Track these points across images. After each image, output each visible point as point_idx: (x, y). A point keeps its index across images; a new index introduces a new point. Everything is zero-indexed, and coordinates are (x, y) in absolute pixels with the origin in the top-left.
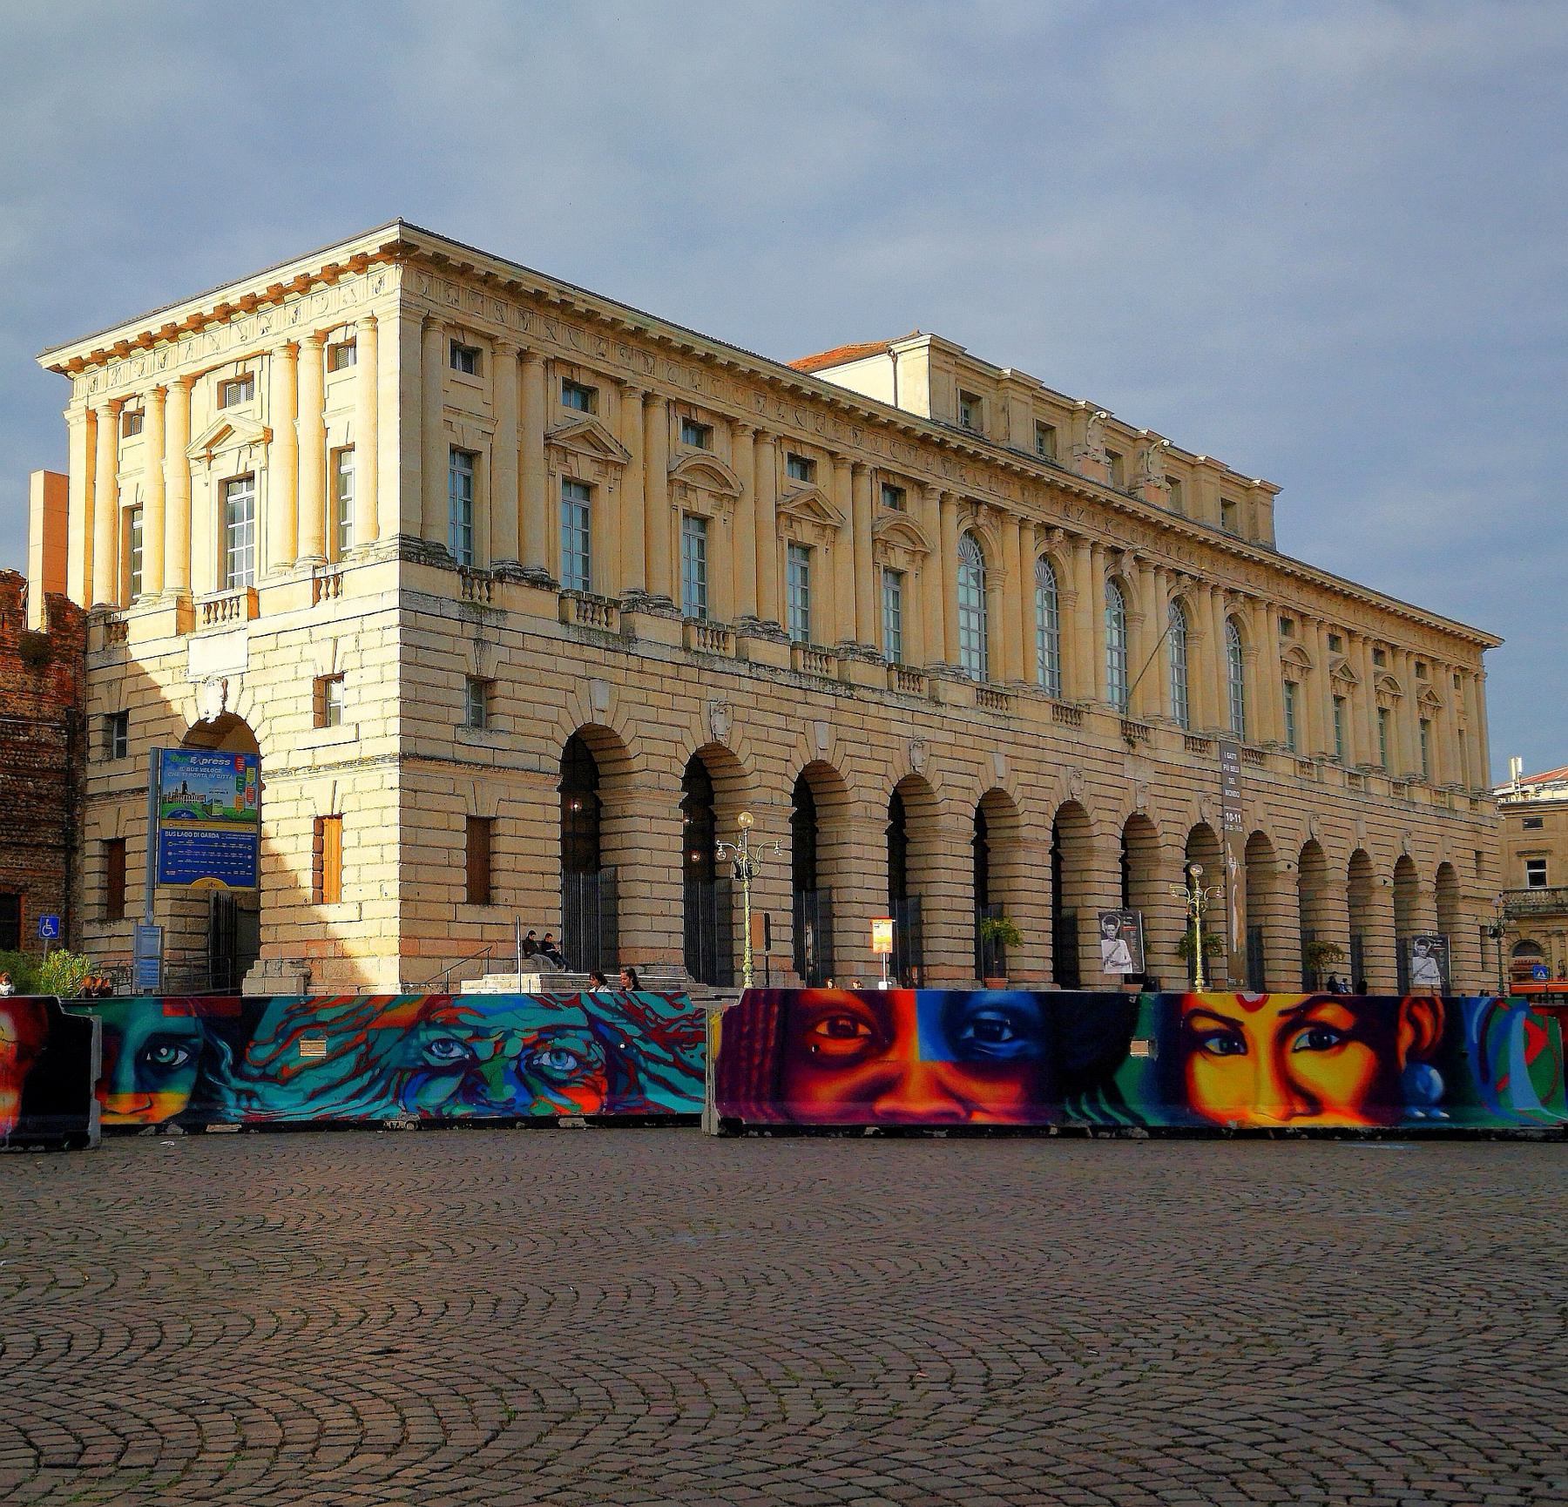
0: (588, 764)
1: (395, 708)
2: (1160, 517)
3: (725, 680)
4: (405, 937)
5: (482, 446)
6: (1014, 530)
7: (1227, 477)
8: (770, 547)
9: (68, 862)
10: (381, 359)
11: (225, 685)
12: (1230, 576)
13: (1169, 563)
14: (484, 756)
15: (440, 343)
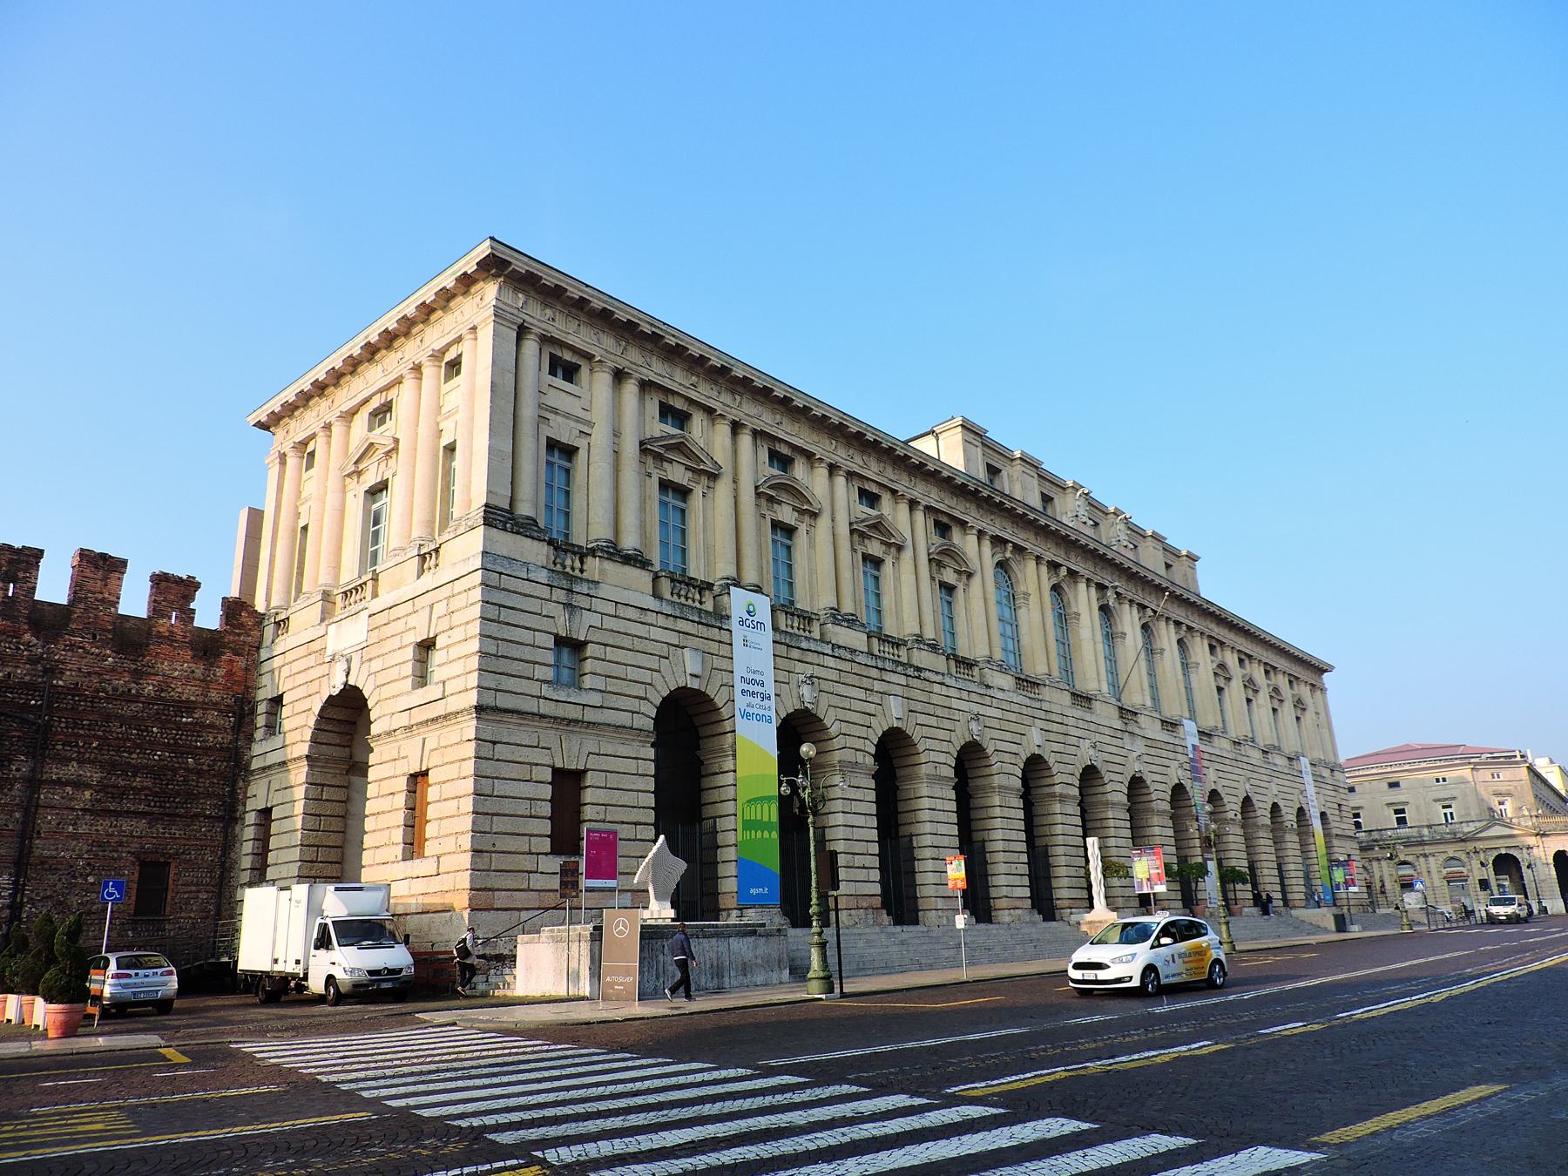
3: (811, 657)
5: (581, 443)
10: (480, 358)
11: (349, 661)
12: (1178, 613)
13: (1139, 599)
14: (573, 713)
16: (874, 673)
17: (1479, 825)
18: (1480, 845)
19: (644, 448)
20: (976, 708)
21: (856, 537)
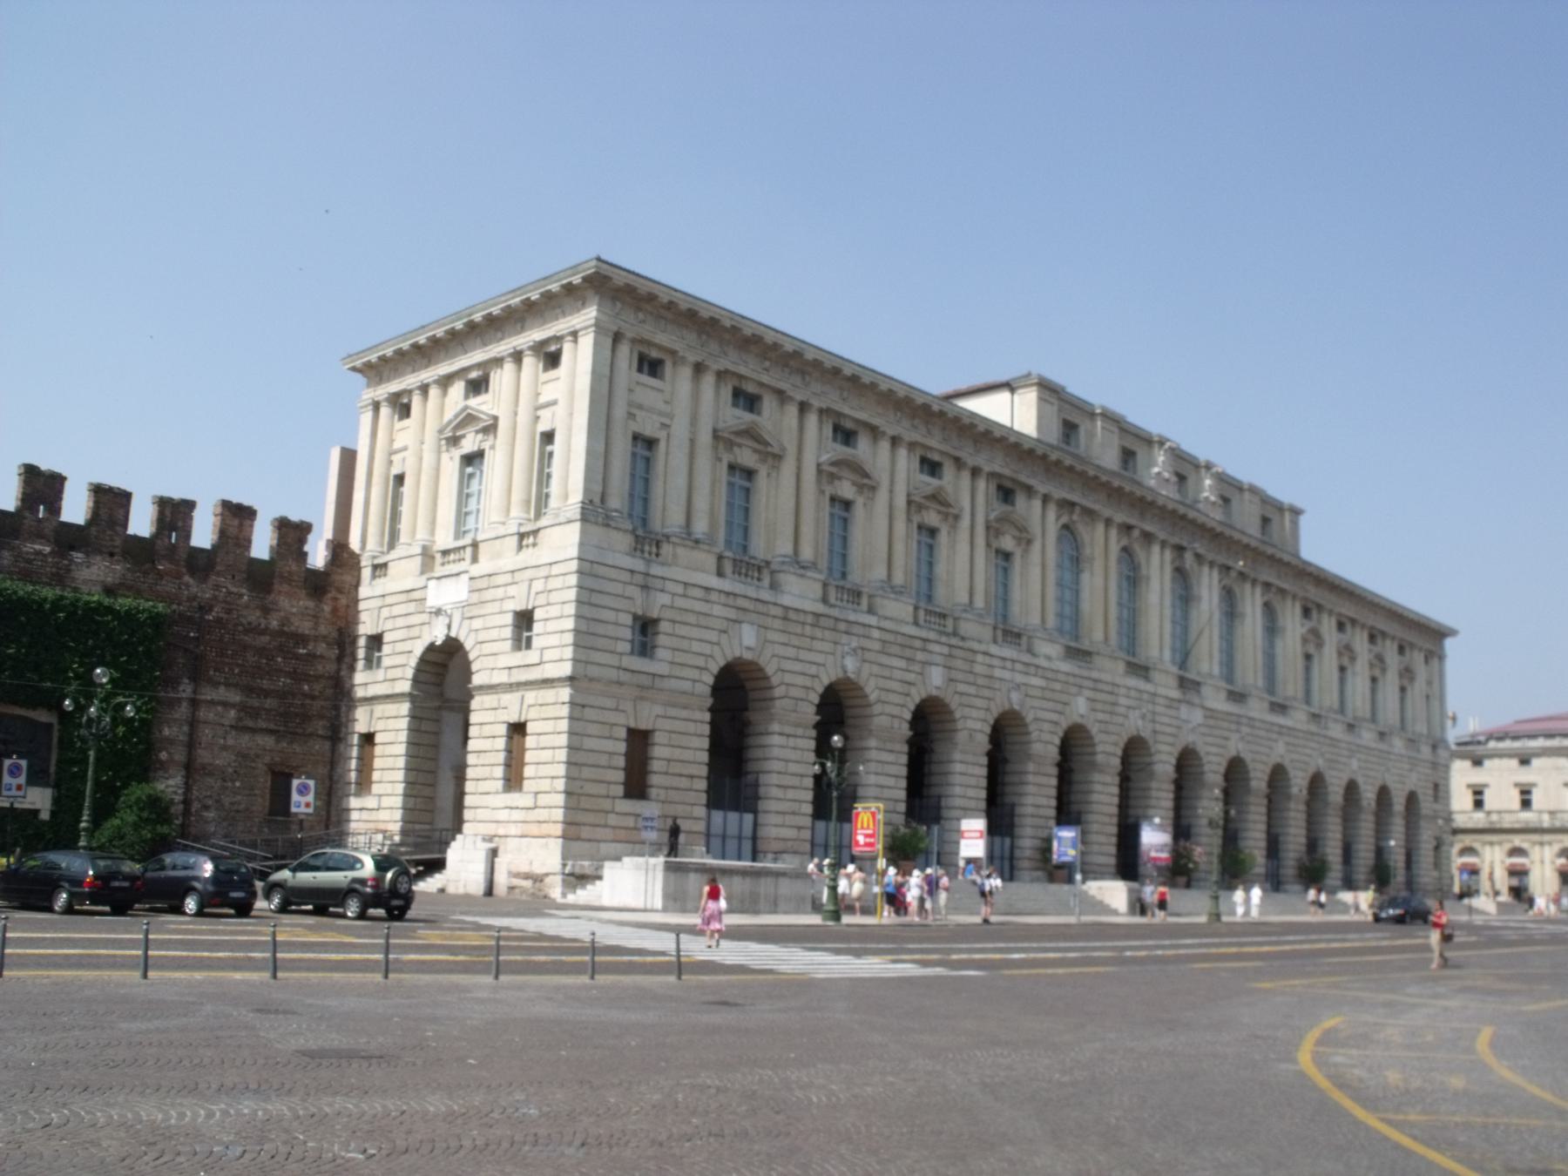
1: (569, 638)
4: (568, 823)
5: (662, 435)
6: (1100, 528)
7: (1266, 501)
8: (900, 526)
9: (333, 750)
10: (580, 359)
11: (450, 617)
12: (1267, 575)
16: (918, 644)
19: (716, 435)
20: (1019, 678)
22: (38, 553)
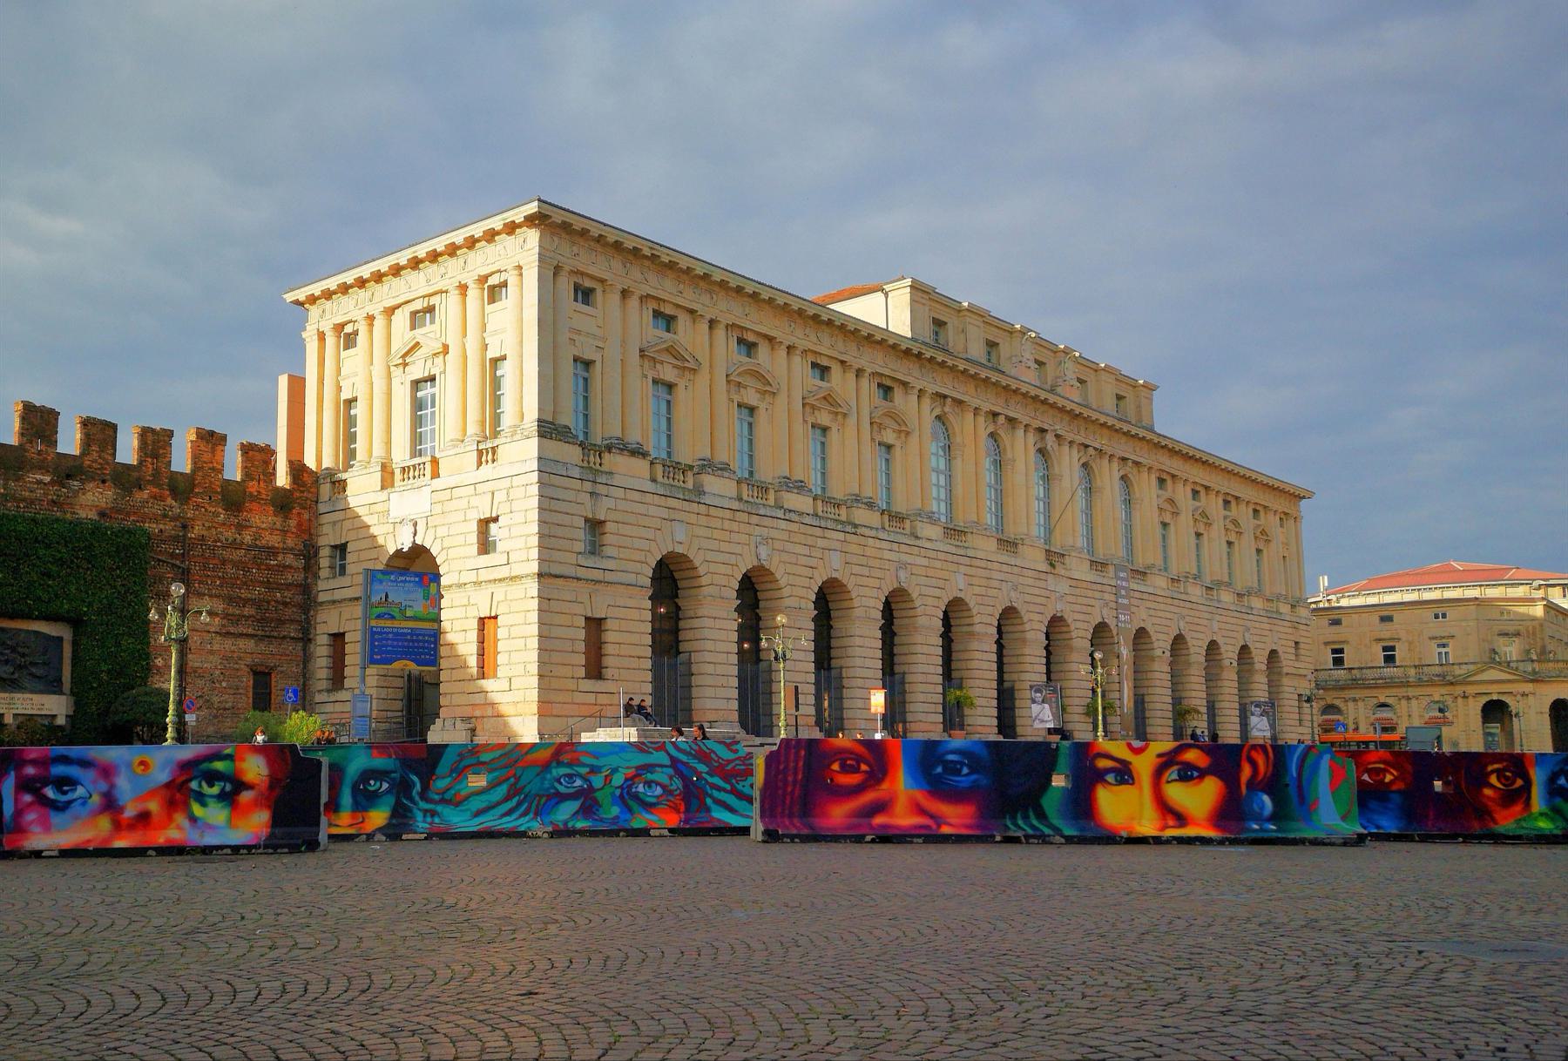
0: (669, 581)
2: (1073, 406)
3: (767, 522)
5: (596, 356)
7: (1120, 378)
8: (799, 428)
10: (526, 296)
11: (415, 525)
13: (1079, 439)
15: (566, 286)
16: (818, 532)
17: (1472, 667)
18: (1471, 690)
21: (808, 409)
22: (39, 482)
